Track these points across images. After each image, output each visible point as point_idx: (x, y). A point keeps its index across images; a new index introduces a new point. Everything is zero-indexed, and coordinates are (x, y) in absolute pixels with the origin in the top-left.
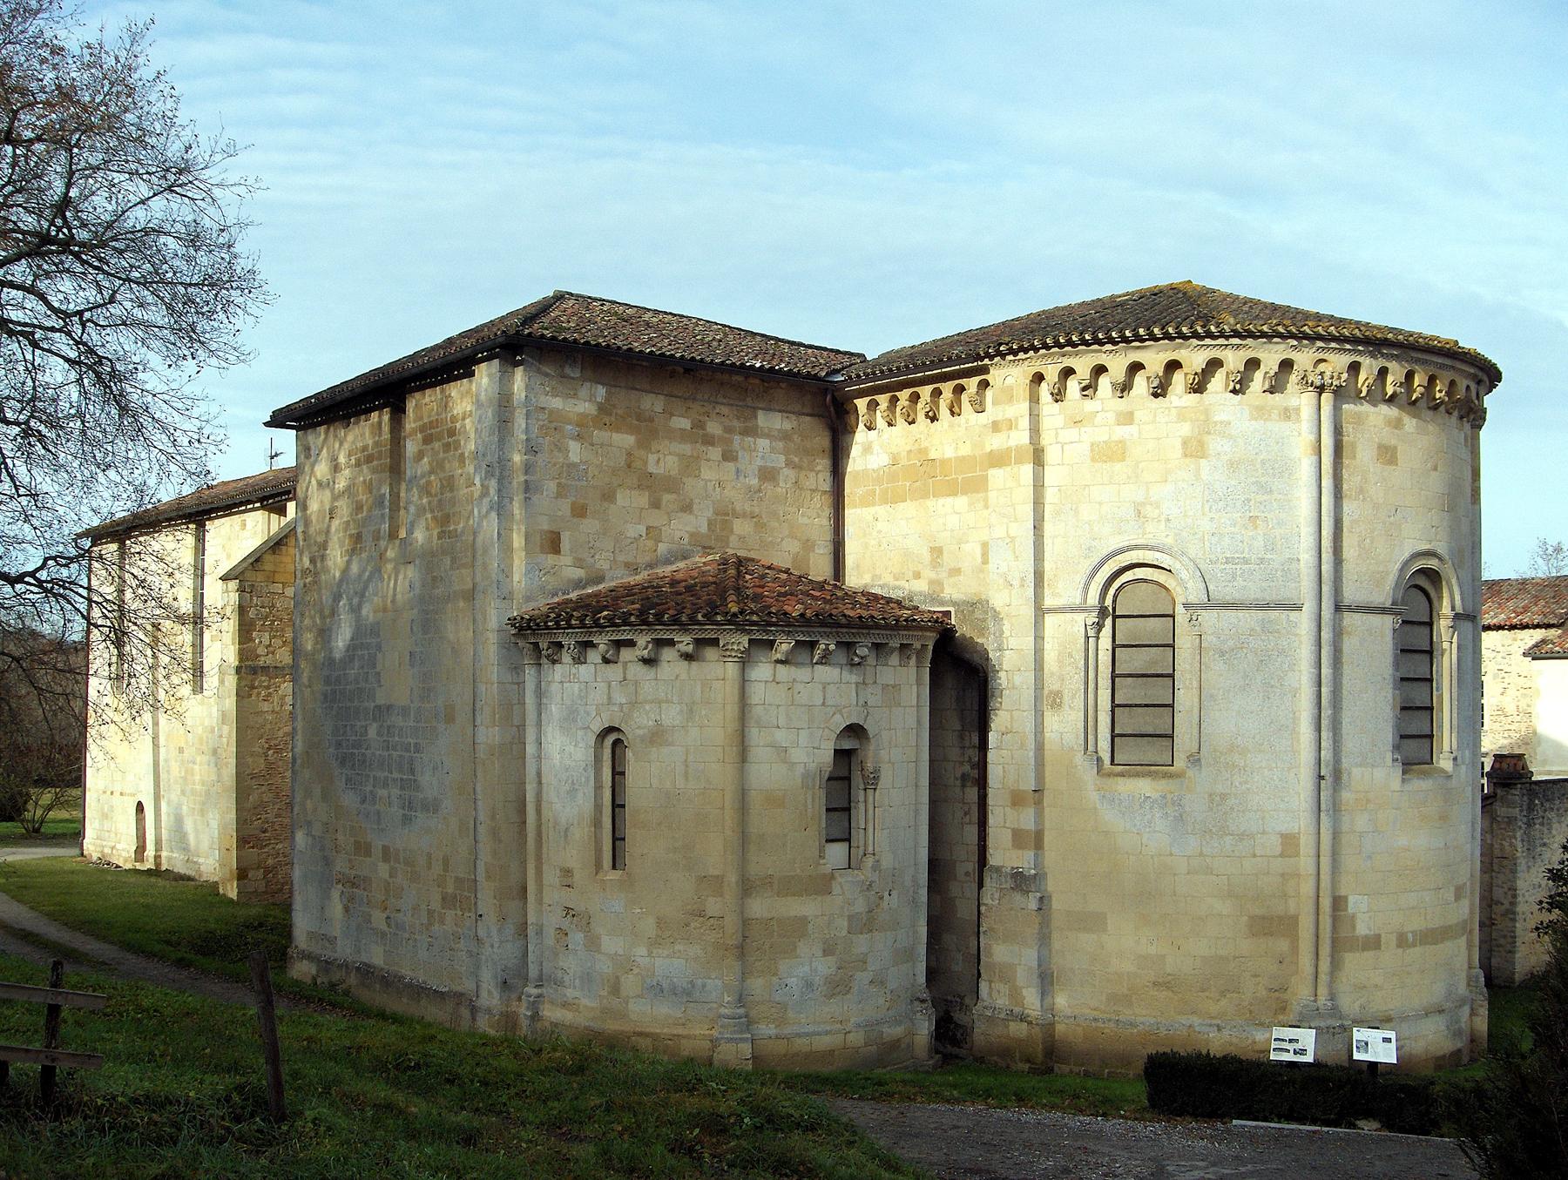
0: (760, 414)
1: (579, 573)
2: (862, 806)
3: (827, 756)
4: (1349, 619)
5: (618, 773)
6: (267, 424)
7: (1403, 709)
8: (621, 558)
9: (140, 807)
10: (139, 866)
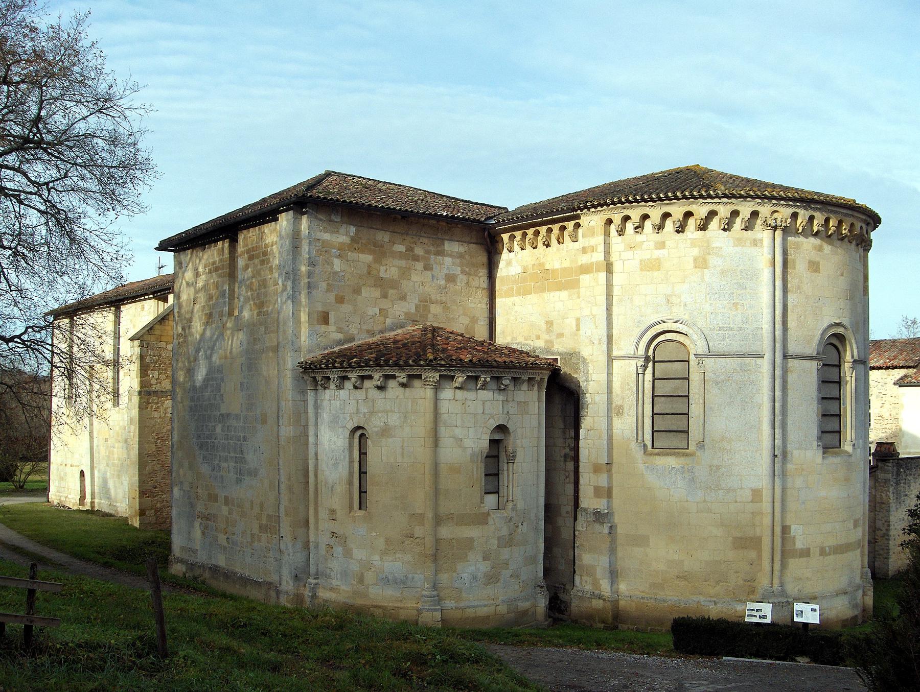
0: (446, 243)
1: (340, 336)
2: (506, 473)
3: (485, 443)
4: (792, 363)
5: (363, 454)
6: (157, 249)
7: (823, 416)
8: (364, 327)
9: (82, 473)
10: (81, 508)
